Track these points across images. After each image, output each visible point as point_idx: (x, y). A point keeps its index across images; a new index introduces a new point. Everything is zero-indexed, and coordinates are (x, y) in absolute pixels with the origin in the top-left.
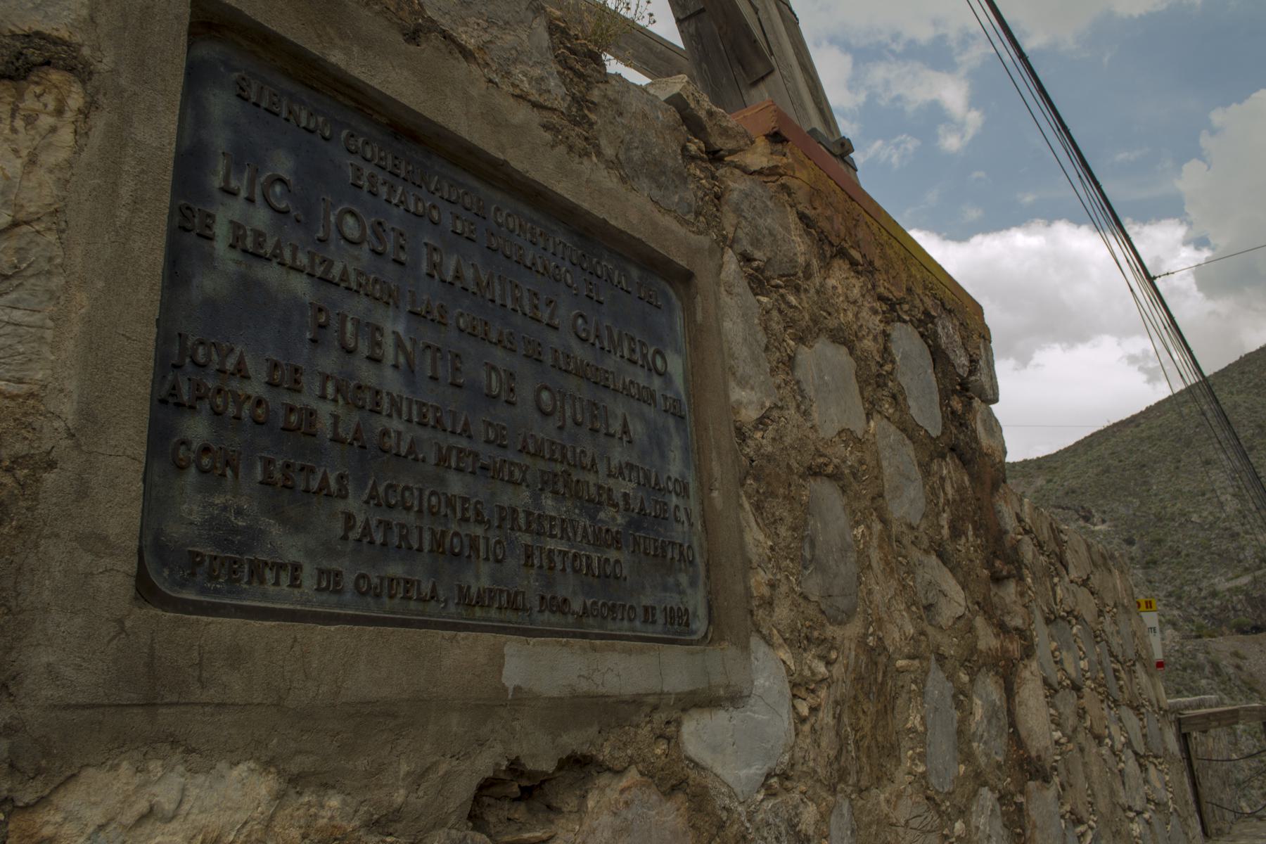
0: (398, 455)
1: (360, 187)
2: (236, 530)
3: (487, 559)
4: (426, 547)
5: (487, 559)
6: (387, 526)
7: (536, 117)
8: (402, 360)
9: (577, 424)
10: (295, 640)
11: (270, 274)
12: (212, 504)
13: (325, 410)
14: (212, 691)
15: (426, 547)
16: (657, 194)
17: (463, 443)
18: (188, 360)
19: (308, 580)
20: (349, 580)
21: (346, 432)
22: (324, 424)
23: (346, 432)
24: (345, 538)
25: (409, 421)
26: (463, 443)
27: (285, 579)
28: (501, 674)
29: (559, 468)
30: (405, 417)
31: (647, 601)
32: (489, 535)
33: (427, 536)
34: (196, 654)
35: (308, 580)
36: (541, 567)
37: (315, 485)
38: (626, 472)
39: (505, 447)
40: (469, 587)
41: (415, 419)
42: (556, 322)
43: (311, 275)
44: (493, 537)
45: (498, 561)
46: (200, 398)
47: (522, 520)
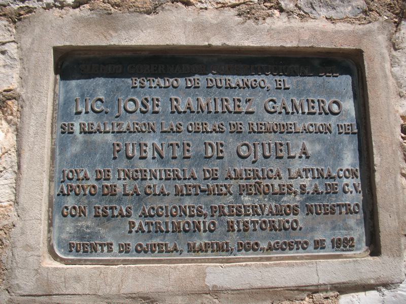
0: (155, 195)
1: (136, 87)
2: (86, 233)
3: (205, 231)
4: (170, 229)
5: (205, 231)
6: (147, 224)
7: (233, 12)
8: (156, 154)
9: (266, 157)
10: (101, 272)
11: (97, 137)
12: (78, 226)
13: (119, 184)
14: (70, 290)
15: (170, 229)
16: (332, 14)
17: (192, 182)
18: (66, 178)
19: (115, 248)
20: (132, 247)
21: (129, 190)
22: (120, 190)
23: (129, 190)
24: (130, 232)
25: (161, 179)
26: (192, 182)
27: (105, 249)
28: (205, 281)
29: (253, 182)
30: (158, 177)
31: (319, 237)
32: (206, 220)
33: (170, 225)
34: (63, 279)
35: (115, 248)
36: (239, 231)
37: (116, 213)
38: (303, 174)
39: (216, 179)
40: (195, 244)
41: (163, 177)
42: (287, 86)
43: (113, 132)
44: (208, 220)
45: (211, 231)
46: (71, 191)
47: (226, 210)
